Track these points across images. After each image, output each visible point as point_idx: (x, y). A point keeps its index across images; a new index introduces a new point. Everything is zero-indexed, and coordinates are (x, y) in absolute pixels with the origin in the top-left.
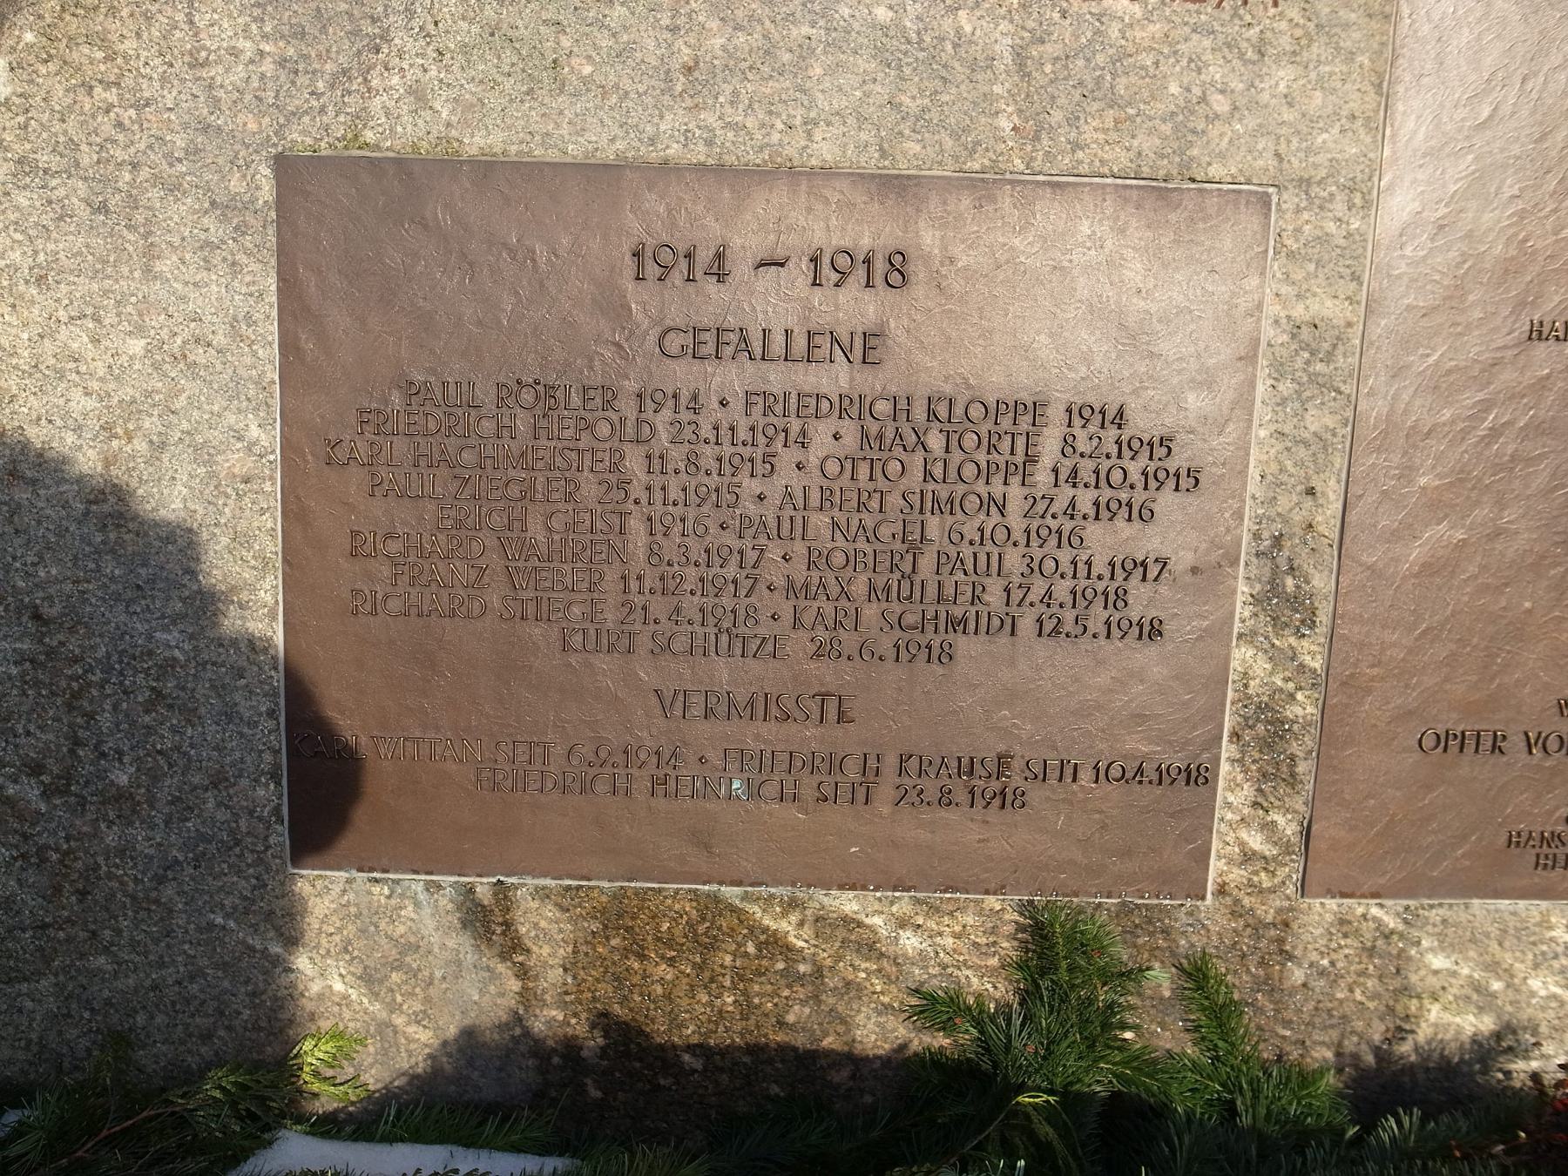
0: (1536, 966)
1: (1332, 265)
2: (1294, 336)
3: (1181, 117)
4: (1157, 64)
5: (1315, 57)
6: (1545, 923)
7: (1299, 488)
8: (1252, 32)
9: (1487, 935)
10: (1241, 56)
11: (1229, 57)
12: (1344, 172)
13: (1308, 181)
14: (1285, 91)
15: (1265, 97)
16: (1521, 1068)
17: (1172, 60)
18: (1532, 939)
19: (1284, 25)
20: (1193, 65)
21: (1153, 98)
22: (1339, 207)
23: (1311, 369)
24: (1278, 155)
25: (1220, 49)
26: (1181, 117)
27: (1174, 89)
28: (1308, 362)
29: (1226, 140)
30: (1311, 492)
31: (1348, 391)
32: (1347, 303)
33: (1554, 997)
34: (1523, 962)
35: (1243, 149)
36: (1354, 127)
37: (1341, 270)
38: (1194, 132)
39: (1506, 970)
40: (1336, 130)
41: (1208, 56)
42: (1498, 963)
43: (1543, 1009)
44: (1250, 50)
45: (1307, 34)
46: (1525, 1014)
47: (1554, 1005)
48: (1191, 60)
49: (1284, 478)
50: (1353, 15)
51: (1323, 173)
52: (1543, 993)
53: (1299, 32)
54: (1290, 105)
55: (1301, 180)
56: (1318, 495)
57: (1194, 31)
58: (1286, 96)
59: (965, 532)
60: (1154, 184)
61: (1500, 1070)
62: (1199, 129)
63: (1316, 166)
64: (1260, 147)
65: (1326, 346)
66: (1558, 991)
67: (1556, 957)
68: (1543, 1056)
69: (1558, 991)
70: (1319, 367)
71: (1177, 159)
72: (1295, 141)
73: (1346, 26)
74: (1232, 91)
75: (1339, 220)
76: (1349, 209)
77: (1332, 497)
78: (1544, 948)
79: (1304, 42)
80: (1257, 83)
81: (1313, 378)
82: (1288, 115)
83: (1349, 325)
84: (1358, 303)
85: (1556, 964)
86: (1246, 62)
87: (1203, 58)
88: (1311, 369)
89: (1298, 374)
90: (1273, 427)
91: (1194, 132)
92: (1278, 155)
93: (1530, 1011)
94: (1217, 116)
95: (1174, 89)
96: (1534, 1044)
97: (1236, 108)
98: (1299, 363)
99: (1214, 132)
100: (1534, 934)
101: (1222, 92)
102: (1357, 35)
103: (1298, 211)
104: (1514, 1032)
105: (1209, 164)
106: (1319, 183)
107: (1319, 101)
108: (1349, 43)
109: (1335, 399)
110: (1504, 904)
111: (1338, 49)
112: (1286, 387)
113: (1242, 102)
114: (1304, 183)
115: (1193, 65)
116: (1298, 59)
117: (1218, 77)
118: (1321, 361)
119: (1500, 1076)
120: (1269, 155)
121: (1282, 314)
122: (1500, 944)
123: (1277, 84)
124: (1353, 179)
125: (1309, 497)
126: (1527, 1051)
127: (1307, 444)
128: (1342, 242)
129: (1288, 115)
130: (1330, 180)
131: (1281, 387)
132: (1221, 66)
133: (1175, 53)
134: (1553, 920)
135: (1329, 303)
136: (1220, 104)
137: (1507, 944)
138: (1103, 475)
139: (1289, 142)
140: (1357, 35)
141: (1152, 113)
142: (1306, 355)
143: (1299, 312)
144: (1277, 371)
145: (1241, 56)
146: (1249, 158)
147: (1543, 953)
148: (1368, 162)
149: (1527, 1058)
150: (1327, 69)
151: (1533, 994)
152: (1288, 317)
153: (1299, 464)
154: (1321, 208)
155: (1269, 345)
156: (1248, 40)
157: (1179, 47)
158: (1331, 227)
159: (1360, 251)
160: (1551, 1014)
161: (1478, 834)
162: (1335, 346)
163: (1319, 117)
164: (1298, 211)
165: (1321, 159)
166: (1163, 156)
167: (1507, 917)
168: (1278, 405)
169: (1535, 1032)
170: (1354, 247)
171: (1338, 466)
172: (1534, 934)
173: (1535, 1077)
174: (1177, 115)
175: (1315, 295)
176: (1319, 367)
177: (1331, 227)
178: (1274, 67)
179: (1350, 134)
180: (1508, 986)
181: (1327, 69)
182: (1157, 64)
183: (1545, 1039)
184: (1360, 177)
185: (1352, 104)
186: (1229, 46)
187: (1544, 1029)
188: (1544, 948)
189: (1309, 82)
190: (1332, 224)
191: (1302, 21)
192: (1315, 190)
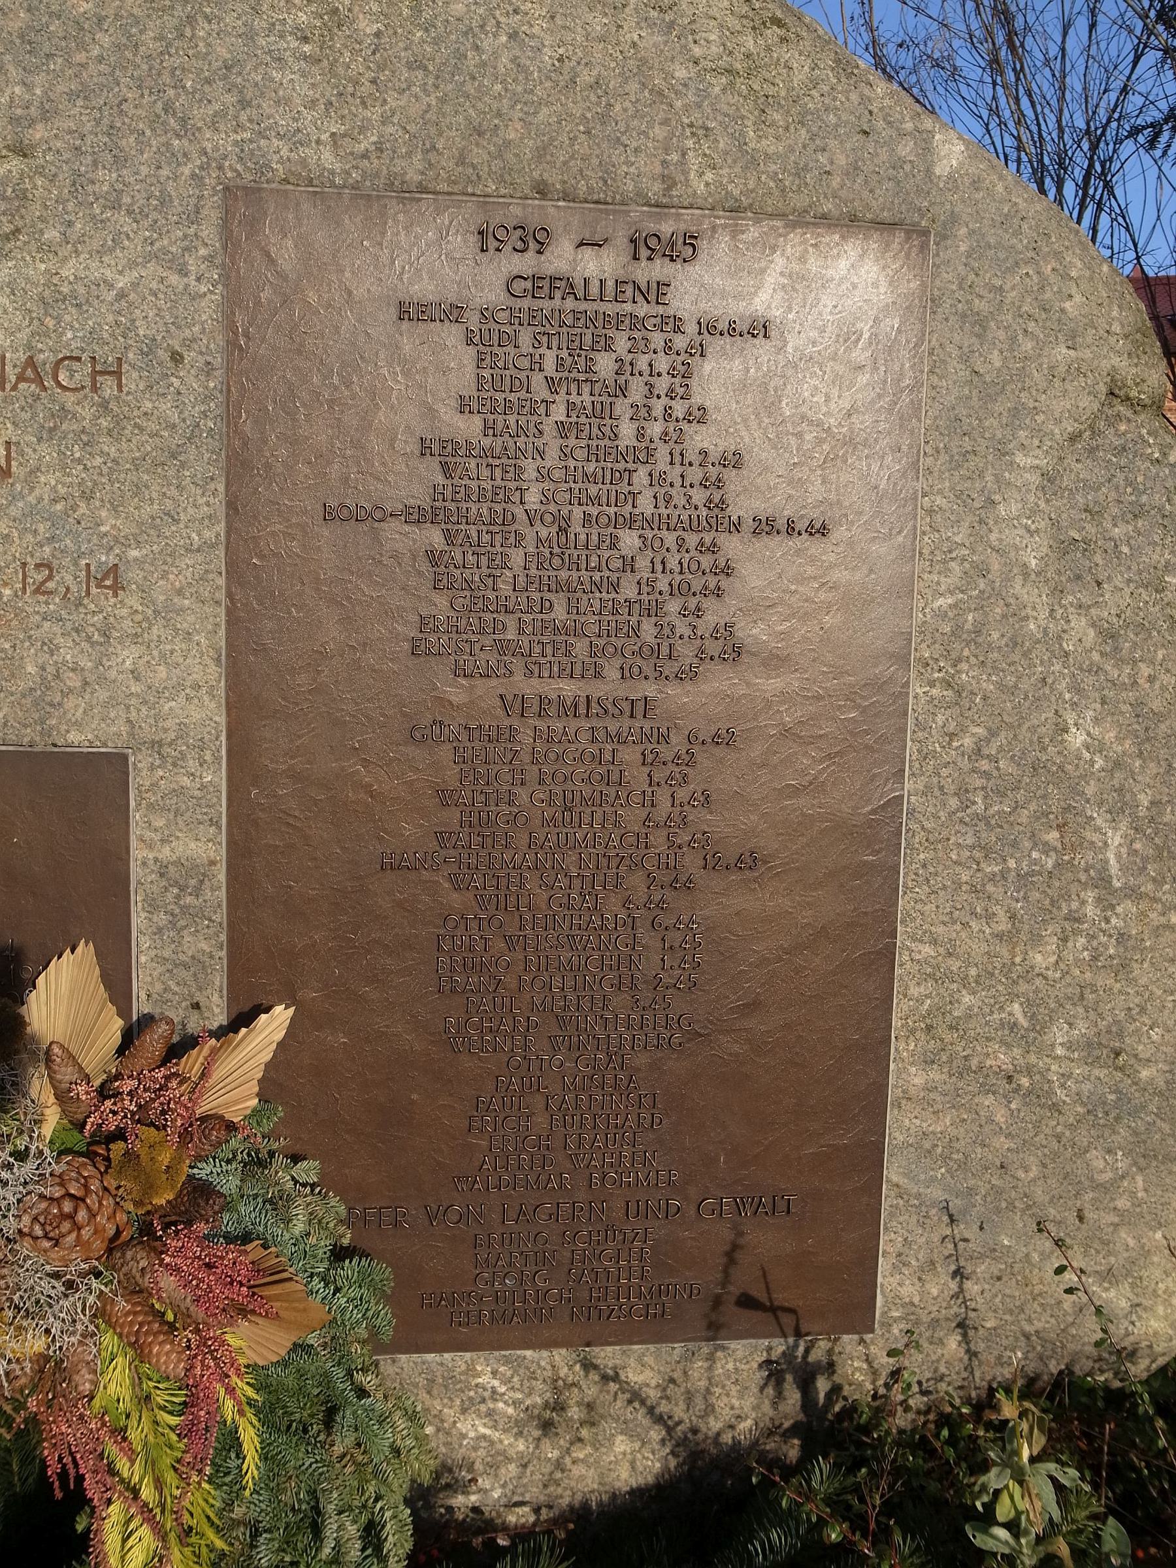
0: (464, 1411)
1: (189, 814)
2: (162, 875)
3: (39, 692)
4: (14, 647)
5: (155, 638)
6: (470, 1371)
7: (184, 1004)
8: (96, 618)
9: (416, 1385)
10: (89, 638)
11: (77, 640)
12: (192, 734)
13: (160, 743)
14: (131, 667)
15: (113, 674)
16: (461, 1502)
17: (27, 644)
18: (458, 1387)
19: (124, 612)
20: (45, 648)
21: (13, 675)
22: (192, 765)
23: (182, 903)
24: (129, 721)
25: (69, 634)
26: (39, 692)
27: (31, 669)
28: (178, 897)
29: (81, 710)
30: (196, 1006)
31: (219, 920)
32: (210, 845)
33: (484, 1437)
34: (451, 1408)
35: (97, 718)
36: (199, 695)
37: (200, 817)
38: (52, 705)
39: (435, 1416)
40: (181, 699)
41: (60, 640)
42: (428, 1409)
43: (475, 1449)
44: (96, 633)
45: (146, 619)
46: (459, 1455)
47: (483, 1444)
48: (44, 644)
49: (169, 996)
50: (187, 602)
51: (173, 735)
52: (472, 1434)
53: (139, 617)
54: (137, 679)
55: (153, 743)
56: (204, 1009)
57: (44, 619)
58: (132, 672)
59: (666, 541)
60: (21, 749)
61: (442, 1506)
62: (56, 701)
63: (166, 730)
64: (112, 715)
65: (193, 882)
66: (488, 1432)
67: (483, 1401)
68: (480, 1491)
69: (488, 1432)
70: (189, 900)
71: (39, 728)
72: (144, 709)
73: (181, 611)
74: (83, 669)
75: (192, 774)
76: (201, 765)
77: (217, 1010)
78: (472, 1393)
79: (145, 625)
80: (104, 660)
81: (185, 909)
82: (135, 688)
83: (212, 863)
84: (220, 844)
85: (483, 1408)
86: (93, 644)
87: (55, 642)
88: (182, 903)
89: (170, 907)
90: (153, 953)
91: (52, 705)
92: (129, 721)
93: (463, 1450)
94: (71, 691)
95: (31, 669)
96: (470, 1481)
97: (87, 683)
98: (169, 897)
99: (70, 703)
100: (460, 1381)
101: (73, 670)
102: (191, 619)
103: (152, 768)
104: (450, 1471)
105: (68, 731)
106: (170, 744)
107: (164, 675)
108: (185, 625)
109: (208, 927)
110: (430, 1357)
111: (176, 630)
112: (162, 918)
113: (91, 678)
114: (157, 745)
115: (45, 648)
116: (140, 640)
117: (68, 657)
118: (191, 894)
119: (442, 1510)
120: (121, 722)
121: (150, 856)
122: (429, 1393)
123: (124, 661)
124: (201, 740)
125: (196, 1012)
126: (465, 1486)
127: (186, 966)
128: (197, 793)
129: (135, 688)
130: (179, 742)
131: (155, 919)
132: (70, 648)
133: (30, 637)
134: (479, 1368)
135: (193, 845)
136: (73, 680)
137: (435, 1392)
138: (685, 565)
139: (139, 710)
140: (191, 619)
141: (14, 688)
142: (176, 891)
143: (166, 853)
144: (150, 905)
145: (89, 638)
146: (103, 725)
147: (471, 1399)
148: (213, 725)
149: (466, 1493)
150: (168, 647)
151: (464, 1436)
152: (156, 860)
153: (182, 983)
154: (175, 765)
155: (139, 882)
156: (93, 625)
157: (32, 632)
158: (186, 781)
159: (215, 800)
160: (481, 1453)
161: (1024, 1022)
162: (202, 882)
163: (165, 688)
164: (152, 768)
165: (169, 723)
166: (25, 726)
167: (434, 1367)
168: (155, 934)
169: (471, 1469)
170: (209, 797)
171: (218, 983)
172: (460, 1381)
173: (476, 1510)
174: (35, 690)
175: (178, 838)
176: (189, 900)
177: (186, 781)
178: (119, 647)
179: (196, 701)
180: (438, 1430)
181: (168, 647)
182: (14, 647)
183: (481, 1475)
184: (207, 737)
185: (195, 676)
186: (77, 631)
187: (478, 1466)
188: (472, 1393)
189: (153, 659)
190: (185, 778)
191: (140, 608)
192: (166, 750)
